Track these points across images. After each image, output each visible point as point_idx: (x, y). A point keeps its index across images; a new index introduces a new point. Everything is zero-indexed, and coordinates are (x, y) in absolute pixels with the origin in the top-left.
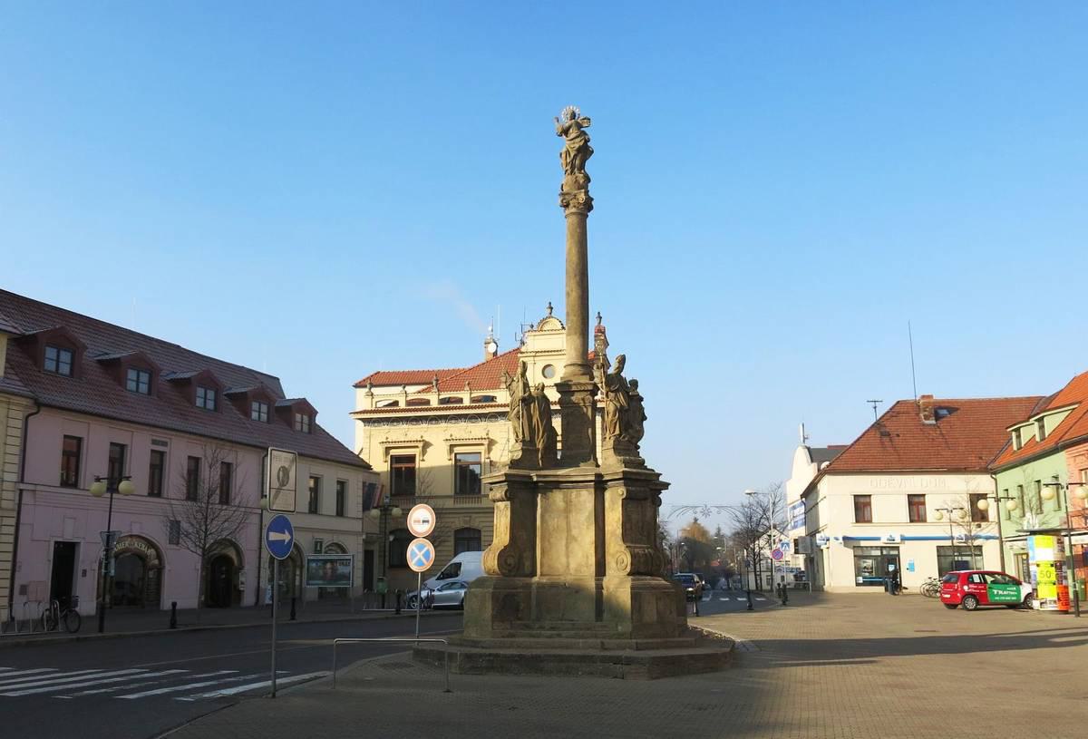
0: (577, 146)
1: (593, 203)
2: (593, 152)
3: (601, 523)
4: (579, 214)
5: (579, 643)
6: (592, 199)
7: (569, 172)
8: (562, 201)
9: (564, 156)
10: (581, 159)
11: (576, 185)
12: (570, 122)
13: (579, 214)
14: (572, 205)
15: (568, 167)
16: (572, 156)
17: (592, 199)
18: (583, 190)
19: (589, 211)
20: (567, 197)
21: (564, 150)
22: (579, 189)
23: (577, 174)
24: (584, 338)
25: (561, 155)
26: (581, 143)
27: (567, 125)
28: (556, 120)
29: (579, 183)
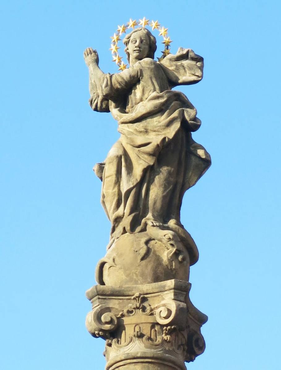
0: (155, 139)
1: (205, 330)
2: (206, 163)
3: (120, 167)
4: (156, 360)
5: (172, 357)
6: (202, 319)
7: (126, 222)
8: (98, 317)
9: (110, 170)
10: (167, 183)
11: (148, 267)
12: (134, 67)
13: (156, 360)
14: (129, 331)
15: (125, 210)
16: (138, 171)
17: (202, 319)
18: (171, 283)
19: (191, 359)
20: (114, 303)
21: (114, 151)
22: (157, 279)
23: (153, 231)
24: (128, 122)
25: (101, 167)
26: (171, 133)
27: (126, 74)
28: (89, 59)
29: (158, 259)
